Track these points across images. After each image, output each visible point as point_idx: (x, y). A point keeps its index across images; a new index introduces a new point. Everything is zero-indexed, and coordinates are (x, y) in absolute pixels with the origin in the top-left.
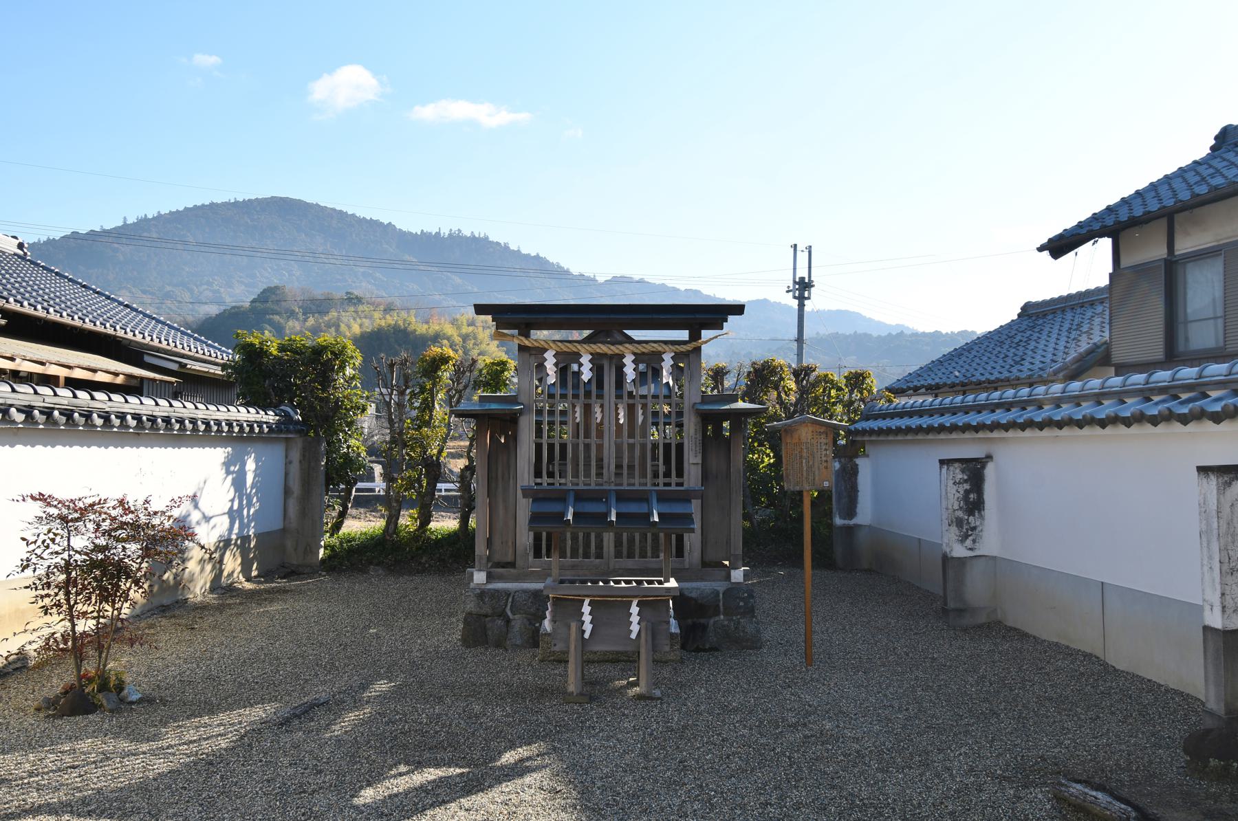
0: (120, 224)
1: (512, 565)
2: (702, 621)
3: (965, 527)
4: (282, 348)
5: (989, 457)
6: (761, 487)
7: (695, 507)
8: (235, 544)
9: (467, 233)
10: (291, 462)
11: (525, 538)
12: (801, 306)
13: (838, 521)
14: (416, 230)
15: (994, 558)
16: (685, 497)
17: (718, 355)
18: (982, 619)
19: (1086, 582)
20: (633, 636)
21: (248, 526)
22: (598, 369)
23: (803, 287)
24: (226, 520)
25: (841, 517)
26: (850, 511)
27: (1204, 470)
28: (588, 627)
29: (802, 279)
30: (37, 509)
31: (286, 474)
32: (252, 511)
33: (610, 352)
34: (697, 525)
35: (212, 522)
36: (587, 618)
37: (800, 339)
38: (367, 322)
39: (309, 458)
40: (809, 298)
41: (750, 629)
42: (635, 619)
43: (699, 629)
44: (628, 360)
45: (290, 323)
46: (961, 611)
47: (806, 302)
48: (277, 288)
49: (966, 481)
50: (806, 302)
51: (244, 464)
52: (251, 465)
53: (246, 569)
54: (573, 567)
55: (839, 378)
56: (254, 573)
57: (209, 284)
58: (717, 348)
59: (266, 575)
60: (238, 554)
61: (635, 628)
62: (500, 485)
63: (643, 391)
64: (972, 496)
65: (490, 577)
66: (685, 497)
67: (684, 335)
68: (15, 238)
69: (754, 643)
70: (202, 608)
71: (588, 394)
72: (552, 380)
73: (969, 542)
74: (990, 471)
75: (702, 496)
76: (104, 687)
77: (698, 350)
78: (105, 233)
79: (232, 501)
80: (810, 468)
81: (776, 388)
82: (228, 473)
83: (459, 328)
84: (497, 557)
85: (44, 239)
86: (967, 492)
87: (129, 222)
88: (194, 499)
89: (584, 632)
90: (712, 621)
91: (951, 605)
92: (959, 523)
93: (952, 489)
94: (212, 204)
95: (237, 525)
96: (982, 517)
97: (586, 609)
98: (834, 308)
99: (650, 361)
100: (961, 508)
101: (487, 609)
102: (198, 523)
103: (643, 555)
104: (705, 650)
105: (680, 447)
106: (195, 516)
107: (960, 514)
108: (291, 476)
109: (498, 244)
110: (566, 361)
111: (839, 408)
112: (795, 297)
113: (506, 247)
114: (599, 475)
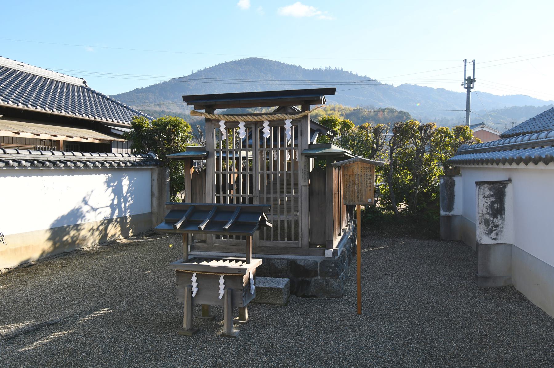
0: (191, 74)
2: (308, 279)
3: (491, 225)
5: (510, 180)
8: (116, 221)
9: (333, 68)
10: (154, 180)
12: (469, 92)
13: (442, 213)
14: (311, 68)
15: (511, 245)
17: (453, 119)
18: (501, 283)
20: (220, 297)
21: (125, 212)
23: (470, 82)
24: (109, 210)
25: (444, 211)
26: (450, 206)
28: (195, 290)
29: (469, 78)
31: (152, 186)
32: (128, 204)
33: (254, 120)
35: (98, 211)
36: (194, 284)
37: (468, 110)
40: (473, 88)
42: (222, 286)
46: (486, 278)
47: (471, 90)
49: (492, 196)
50: (471, 90)
51: (120, 182)
53: (124, 232)
54: (237, 244)
55: (451, 131)
56: (130, 234)
59: (138, 235)
60: (117, 226)
61: (222, 292)
62: (198, 196)
64: (496, 205)
68: (82, 79)
69: (338, 295)
70: (91, 254)
73: (493, 235)
74: (509, 190)
78: (185, 78)
79: (113, 200)
80: (359, 190)
82: (109, 186)
83: (326, 111)
85: (162, 82)
86: (493, 203)
87: (194, 72)
88: (85, 202)
89: (192, 292)
90: (313, 279)
91: (480, 274)
92: (487, 222)
93: (482, 201)
94: (226, 63)
95: (117, 211)
96: (503, 219)
97: (194, 279)
98: (515, 94)
100: (488, 213)
102: (88, 212)
103: (275, 238)
104: (308, 297)
106: (85, 208)
107: (487, 217)
108: (154, 187)
109: (347, 72)
112: (465, 88)
113: (351, 73)
114: (251, 192)
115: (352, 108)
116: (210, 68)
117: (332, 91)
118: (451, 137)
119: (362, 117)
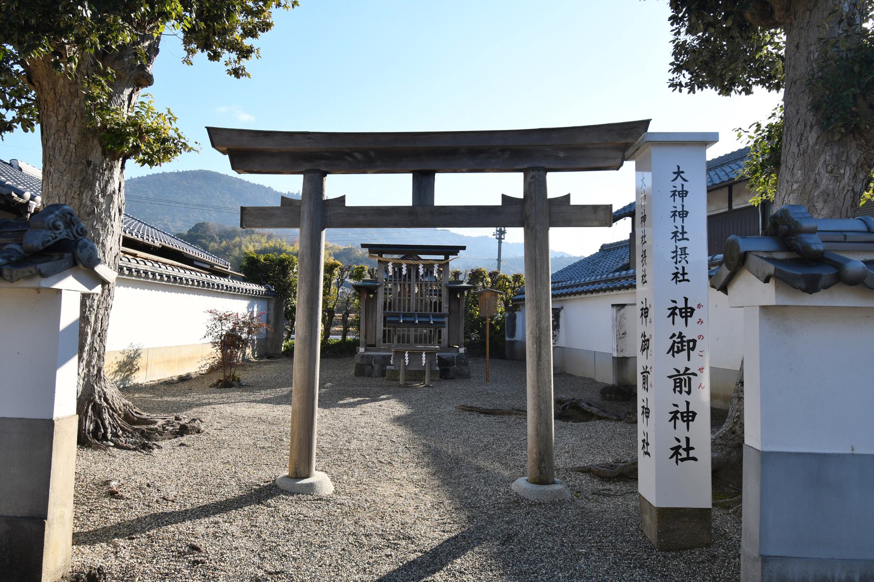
1: (374, 346)
4: (265, 260)
5: (562, 308)
6: (474, 324)
7: (446, 320)
11: (380, 335)
12: (500, 243)
13: (507, 339)
16: (443, 316)
19: (589, 352)
22: (409, 270)
26: (513, 334)
27: (613, 305)
28: (407, 362)
30: (212, 317)
34: (447, 326)
36: (407, 358)
37: (499, 260)
38: (257, 244)
39: (278, 307)
41: (466, 371)
42: (424, 359)
43: (447, 371)
44: (421, 267)
45: (212, 244)
48: (204, 223)
52: (256, 309)
53: (253, 354)
55: (510, 277)
57: (162, 220)
58: (456, 263)
59: (260, 357)
61: (424, 362)
63: (427, 279)
65: (366, 350)
66: (443, 316)
67: (442, 257)
71: (405, 280)
72: (391, 274)
74: (562, 313)
75: (449, 316)
76: (234, 380)
77: (448, 263)
81: (482, 281)
84: (369, 343)
97: (407, 355)
99: (429, 267)
101: (365, 362)
105: (440, 303)
110: (398, 266)
111: (509, 291)
115: (342, 247)
116: (139, 178)
117: (464, 248)
118: (510, 282)
119: (354, 258)
